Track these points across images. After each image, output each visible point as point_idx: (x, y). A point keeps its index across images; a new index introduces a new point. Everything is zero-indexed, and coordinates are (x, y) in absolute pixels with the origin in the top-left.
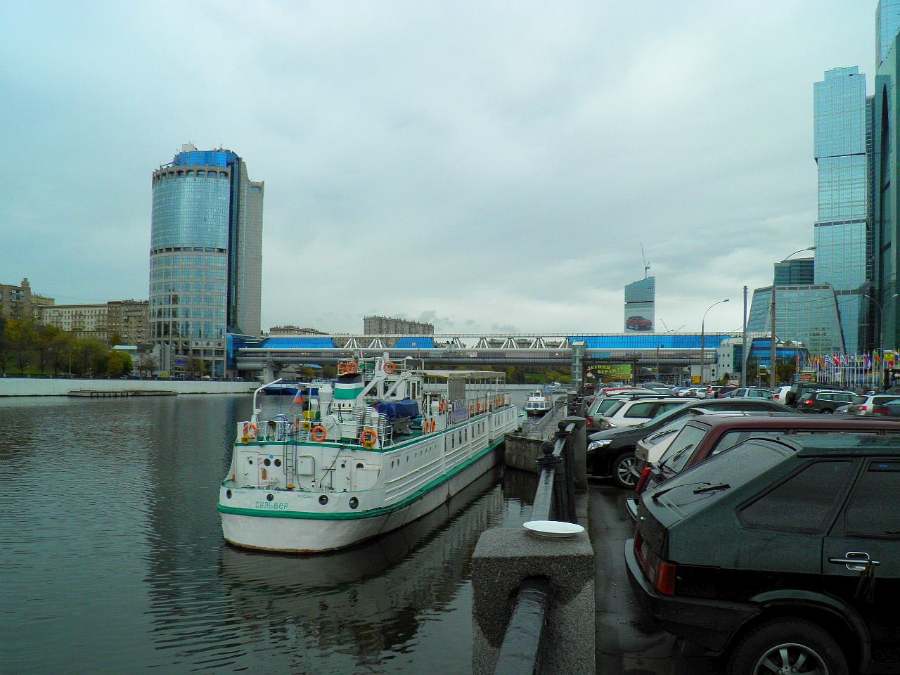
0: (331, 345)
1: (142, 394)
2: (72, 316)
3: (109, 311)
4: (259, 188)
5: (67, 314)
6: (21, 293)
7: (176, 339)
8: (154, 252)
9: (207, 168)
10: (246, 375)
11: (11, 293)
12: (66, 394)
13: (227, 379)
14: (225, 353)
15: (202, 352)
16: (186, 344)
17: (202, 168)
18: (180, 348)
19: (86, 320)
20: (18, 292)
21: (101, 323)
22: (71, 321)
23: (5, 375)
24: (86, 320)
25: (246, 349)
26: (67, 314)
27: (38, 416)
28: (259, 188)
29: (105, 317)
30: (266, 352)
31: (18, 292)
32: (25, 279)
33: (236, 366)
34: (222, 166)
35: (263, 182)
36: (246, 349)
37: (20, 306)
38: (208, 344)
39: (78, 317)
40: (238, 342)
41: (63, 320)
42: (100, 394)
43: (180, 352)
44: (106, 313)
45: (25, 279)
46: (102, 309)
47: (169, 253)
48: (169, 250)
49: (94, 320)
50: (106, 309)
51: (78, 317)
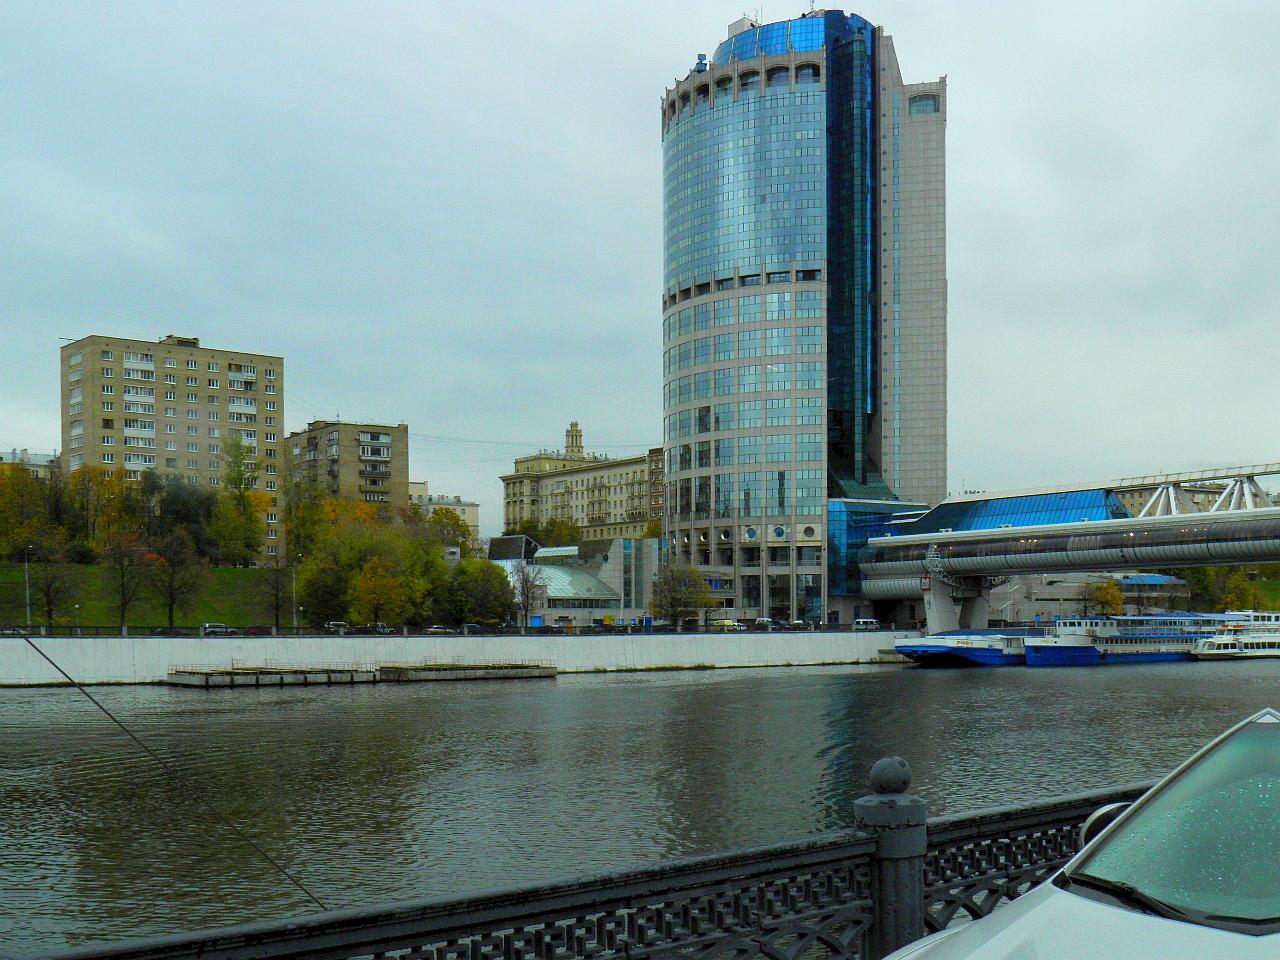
0: (1102, 511)
1: (412, 675)
2: (588, 489)
3: (651, 473)
4: (931, 99)
5: (580, 488)
6: (384, 439)
7: (703, 524)
8: (671, 300)
9: (761, 64)
10: (892, 612)
11: (358, 441)
12: (165, 678)
13: (834, 625)
14: (824, 554)
15: (793, 555)
16: (727, 534)
17: (752, 64)
18: (713, 548)
19: (612, 498)
20: (375, 437)
21: (636, 501)
22: (586, 502)
23: (125, 629)
24: (612, 498)
25: (889, 539)
26: (580, 488)
27: (542, 723)
28: (931, 99)
29: (645, 487)
30: (926, 546)
31: (375, 437)
32: (574, 425)
33: (859, 590)
34: (816, 50)
35: (943, 80)
36: (889, 539)
37: (383, 469)
38: (809, 531)
39: (596, 492)
40: (865, 523)
41: (573, 503)
42: (239, 680)
43: (713, 557)
44: (646, 478)
45: (574, 425)
46: (638, 468)
47: (704, 298)
48: (703, 288)
49: (625, 496)
50: (645, 467)
51: (596, 492)
